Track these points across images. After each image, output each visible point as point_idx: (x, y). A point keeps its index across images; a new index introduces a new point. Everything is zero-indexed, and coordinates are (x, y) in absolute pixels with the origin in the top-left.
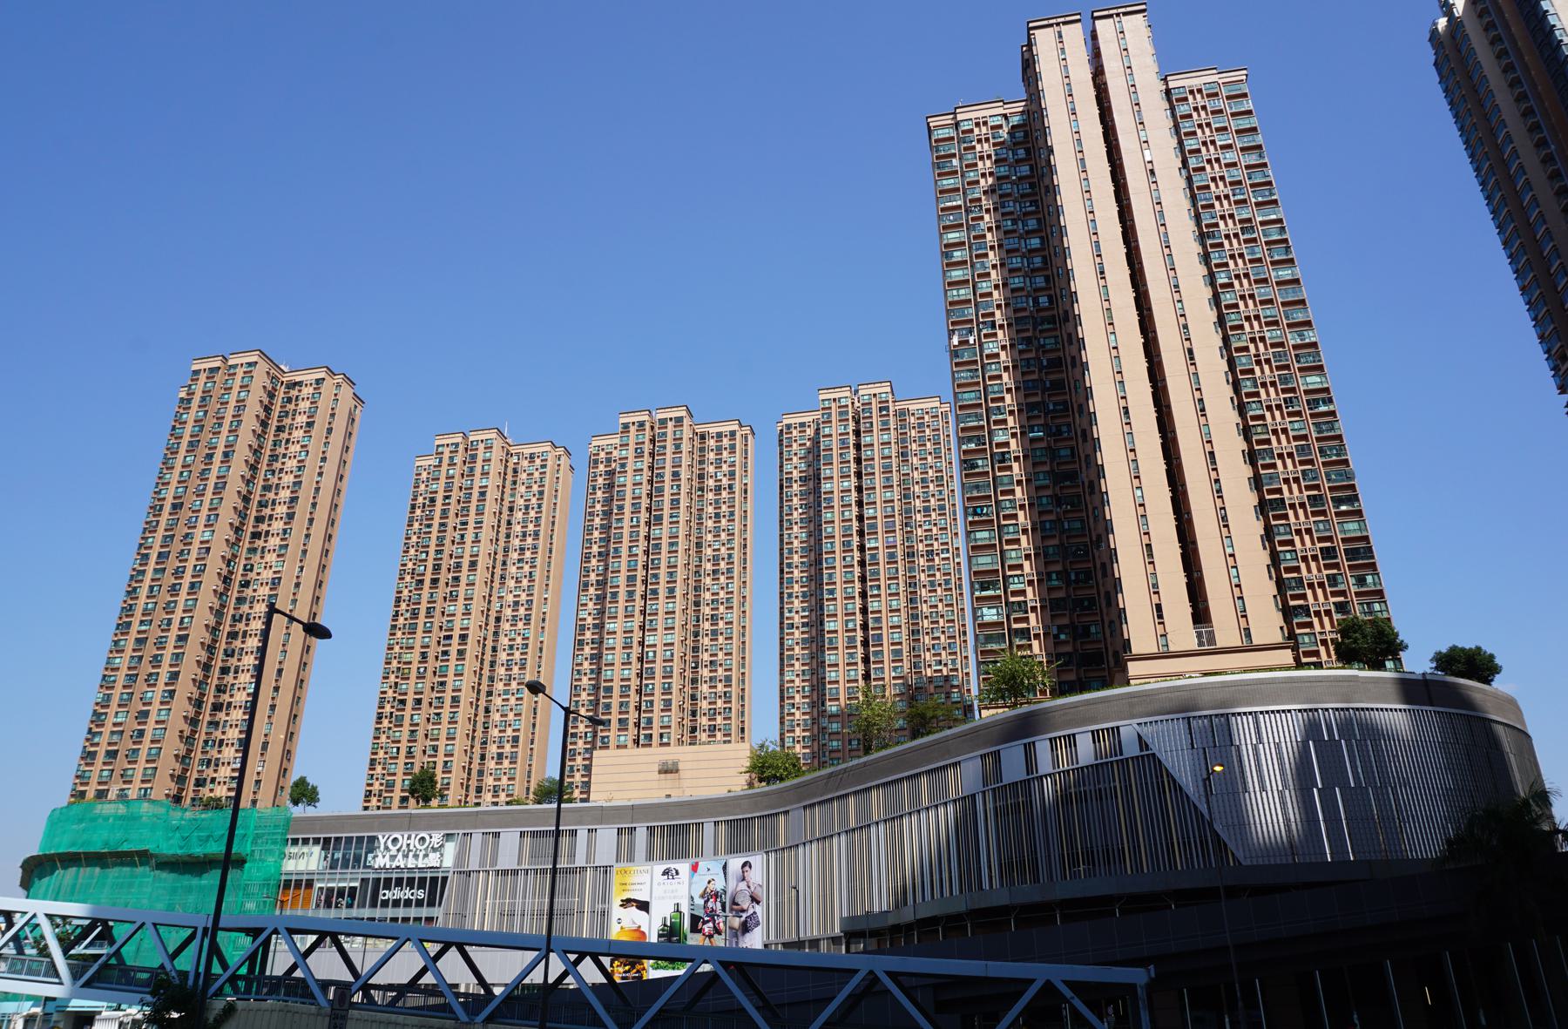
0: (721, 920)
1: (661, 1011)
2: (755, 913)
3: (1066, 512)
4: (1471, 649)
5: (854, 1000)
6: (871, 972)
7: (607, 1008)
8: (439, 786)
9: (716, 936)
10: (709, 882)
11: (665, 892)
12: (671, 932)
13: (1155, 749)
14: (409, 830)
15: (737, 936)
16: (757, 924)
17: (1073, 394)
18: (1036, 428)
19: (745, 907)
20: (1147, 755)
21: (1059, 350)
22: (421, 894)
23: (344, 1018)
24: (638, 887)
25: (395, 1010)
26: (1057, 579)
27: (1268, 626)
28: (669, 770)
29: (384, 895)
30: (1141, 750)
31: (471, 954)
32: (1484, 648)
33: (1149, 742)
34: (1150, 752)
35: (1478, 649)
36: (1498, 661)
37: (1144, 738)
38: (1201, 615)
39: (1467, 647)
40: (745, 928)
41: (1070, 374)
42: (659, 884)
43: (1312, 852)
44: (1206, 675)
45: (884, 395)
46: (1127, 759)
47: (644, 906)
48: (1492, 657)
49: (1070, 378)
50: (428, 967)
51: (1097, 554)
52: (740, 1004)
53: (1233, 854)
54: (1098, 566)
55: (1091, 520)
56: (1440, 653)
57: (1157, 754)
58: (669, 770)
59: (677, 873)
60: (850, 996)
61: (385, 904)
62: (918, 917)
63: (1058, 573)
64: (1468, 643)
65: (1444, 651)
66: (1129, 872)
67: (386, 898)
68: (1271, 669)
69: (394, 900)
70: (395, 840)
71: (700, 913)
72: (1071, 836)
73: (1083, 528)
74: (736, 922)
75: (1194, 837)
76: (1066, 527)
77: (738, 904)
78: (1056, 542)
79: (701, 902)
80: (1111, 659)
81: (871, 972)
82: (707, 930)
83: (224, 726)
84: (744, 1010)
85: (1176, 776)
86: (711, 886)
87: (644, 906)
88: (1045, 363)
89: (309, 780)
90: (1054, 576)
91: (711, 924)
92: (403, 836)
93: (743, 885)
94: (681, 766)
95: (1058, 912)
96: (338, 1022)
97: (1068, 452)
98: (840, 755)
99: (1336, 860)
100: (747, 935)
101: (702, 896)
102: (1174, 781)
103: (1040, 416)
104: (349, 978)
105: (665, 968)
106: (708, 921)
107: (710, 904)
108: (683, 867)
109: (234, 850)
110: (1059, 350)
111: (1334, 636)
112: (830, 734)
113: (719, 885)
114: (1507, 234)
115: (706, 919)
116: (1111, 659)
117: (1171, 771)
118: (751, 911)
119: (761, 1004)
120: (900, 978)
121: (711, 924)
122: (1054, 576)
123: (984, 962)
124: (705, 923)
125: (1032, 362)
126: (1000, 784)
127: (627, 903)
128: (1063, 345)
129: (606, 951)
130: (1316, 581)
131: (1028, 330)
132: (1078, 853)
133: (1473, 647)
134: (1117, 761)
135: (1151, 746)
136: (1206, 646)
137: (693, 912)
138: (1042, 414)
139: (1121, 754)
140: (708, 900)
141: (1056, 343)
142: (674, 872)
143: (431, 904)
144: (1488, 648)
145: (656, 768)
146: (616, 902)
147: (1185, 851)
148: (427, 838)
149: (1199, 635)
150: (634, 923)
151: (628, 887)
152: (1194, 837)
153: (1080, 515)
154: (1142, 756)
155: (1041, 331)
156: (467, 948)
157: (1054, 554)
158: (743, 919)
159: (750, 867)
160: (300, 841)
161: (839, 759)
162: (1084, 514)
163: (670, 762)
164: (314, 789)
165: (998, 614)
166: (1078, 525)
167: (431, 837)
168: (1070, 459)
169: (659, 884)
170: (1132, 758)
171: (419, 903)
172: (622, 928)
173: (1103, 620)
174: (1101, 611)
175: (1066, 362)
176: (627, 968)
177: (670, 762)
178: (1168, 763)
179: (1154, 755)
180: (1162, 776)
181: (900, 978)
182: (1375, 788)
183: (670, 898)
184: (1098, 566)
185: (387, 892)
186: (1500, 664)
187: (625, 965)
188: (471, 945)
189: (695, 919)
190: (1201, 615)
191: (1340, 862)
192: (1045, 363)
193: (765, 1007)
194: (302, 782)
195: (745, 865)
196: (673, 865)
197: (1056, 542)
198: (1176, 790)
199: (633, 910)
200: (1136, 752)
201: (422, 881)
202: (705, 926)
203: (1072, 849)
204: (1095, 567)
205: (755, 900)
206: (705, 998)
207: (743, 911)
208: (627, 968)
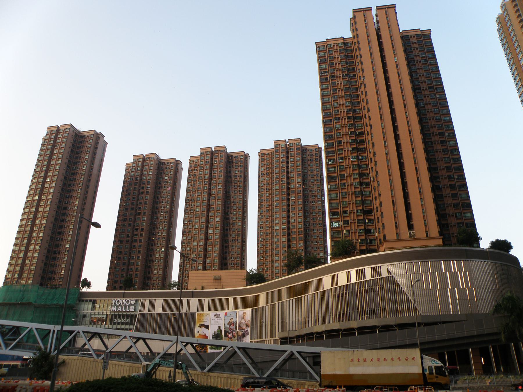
0: (235, 332)
1: (216, 363)
2: (247, 330)
3: (364, 188)
4: (503, 240)
5: (285, 361)
6: (292, 352)
7: (196, 362)
8: (133, 282)
9: (233, 338)
10: (231, 319)
11: (215, 322)
12: (217, 336)
13: (393, 274)
14: (123, 298)
15: (241, 338)
16: (248, 334)
17: (367, 145)
18: (354, 157)
19: (244, 328)
20: (390, 276)
21: (362, 129)
22: (128, 321)
23: (108, 363)
24: (206, 320)
25: (121, 360)
26: (360, 212)
27: (434, 230)
28: (218, 279)
29: (115, 320)
30: (388, 274)
31: (147, 342)
32: (507, 240)
33: (391, 272)
34: (391, 275)
35: (506, 240)
36: (512, 245)
37: (389, 270)
38: (410, 227)
39: (502, 240)
40: (244, 336)
41: (366, 138)
42: (213, 319)
43: (465, 310)
44: (412, 248)
45: (298, 144)
46: (383, 278)
47: (207, 327)
48: (510, 243)
49: (366, 139)
50: (133, 346)
51: (375, 203)
52: (243, 361)
53: (418, 311)
54: (375, 208)
55: (373, 191)
56: (492, 241)
57: (394, 276)
58: (218, 279)
59: (219, 316)
60: (284, 360)
61: (115, 324)
62: (306, 333)
63: (360, 210)
64: (502, 238)
65: (494, 241)
66: (406, 316)
67: (115, 321)
68: (435, 246)
69: (122, 322)
70: (118, 301)
71: (228, 330)
72: (362, 304)
73: (370, 194)
74: (241, 333)
75: (405, 305)
76: (364, 193)
77: (241, 327)
78: (360, 199)
79: (228, 326)
80: (378, 241)
81: (292, 352)
82: (230, 336)
83: (58, 259)
84: (245, 364)
85: (400, 284)
86: (232, 320)
87: (207, 327)
88: (357, 133)
89: (88, 279)
90: (359, 211)
91: (231, 334)
92: (121, 300)
93: (243, 321)
94: (222, 278)
95: (357, 331)
96: (106, 364)
97: (365, 166)
98: (279, 275)
99: (462, 313)
100: (245, 338)
101: (228, 324)
102: (399, 286)
103: (355, 153)
104: (104, 348)
105: (214, 349)
106: (230, 333)
107: (231, 327)
108: (222, 313)
109: (176, 337)
110: (362, 129)
111: (456, 235)
112: (275, 267)
113: (234, 320)
114: (521, 93)
115: (230, 332)
116: (378, 241)
117: (398, 282)
118: (246, 330)
119: (251, 362)
120: (301, 354)
121: (231, 334)
122: (359, 211)
123: (332, 348)
124: (229, 333)
125: (353, 133)
126: (323, 290)
127: (201, 326)
128: (364, 127)
129: (196, 342)
130: (451, 215)
131: (351, 121)
132: (364, 311)
133: (504, 240)
134: (379, 278)
135: (392, 273)
136: (412, 238)
137: (226, 330)
138: (356, 152)
139: (381, 276)
140: (230, 325)
141: (362, 126)
142: (218, 315)
143: (131, 324)
144: (509, 240)
145: (212, 278)
146: (197, 326)
147: (402, 310)
148: (130, 301)
149: (410, 233)
150: (204, 333)
151: (201, 320)
152: (405, 305)
153: (368, 189)
154: (389, 277)
155: (356, 122)
156: (146, 340)
157: (359, 203)
158: (243, 332)
159: (246, 314)
160: (81, 301)
161: (278, 276)
162: (370, 189)
163: (217, 276)
164: (90, 282)
165: (338, 225)
166: (368, 193)
167: (131, 301)
168: (366, 169)
169: (213, 319)
170: (385, 277)
171: (127, 324)
172: (199, 334)
173: (376, 228)
174: (376, 224)
175: (365, 133)
176: (201, 348)
177: (217, 276)
178: (397, 279)
179: (393, 276)
180: (395, 284)
181: (301, 354)
182: (469, 289)
183: (217, 324)
184: (375, 208)
185: (116, 319)
186: (513, 246)
187: (200, 348)
188: (149, 339)
189: (226, 332)
190: (410, 227)
191: (455, 315)
192: (357, 133)
193: (253, 363)
194: (85, 280)
195: (243, 314)
196: (218, 312)
197: (360, 199)
198: (400, 289)
199: (203, 328)
200: (386, 275)
201: (128, 316)
202: (229, 335)
203: (362, 309)
204: (374, 208)
205: (247, 326)
206: (231, 359)
207: (243, 329)
208: (201, 348)
